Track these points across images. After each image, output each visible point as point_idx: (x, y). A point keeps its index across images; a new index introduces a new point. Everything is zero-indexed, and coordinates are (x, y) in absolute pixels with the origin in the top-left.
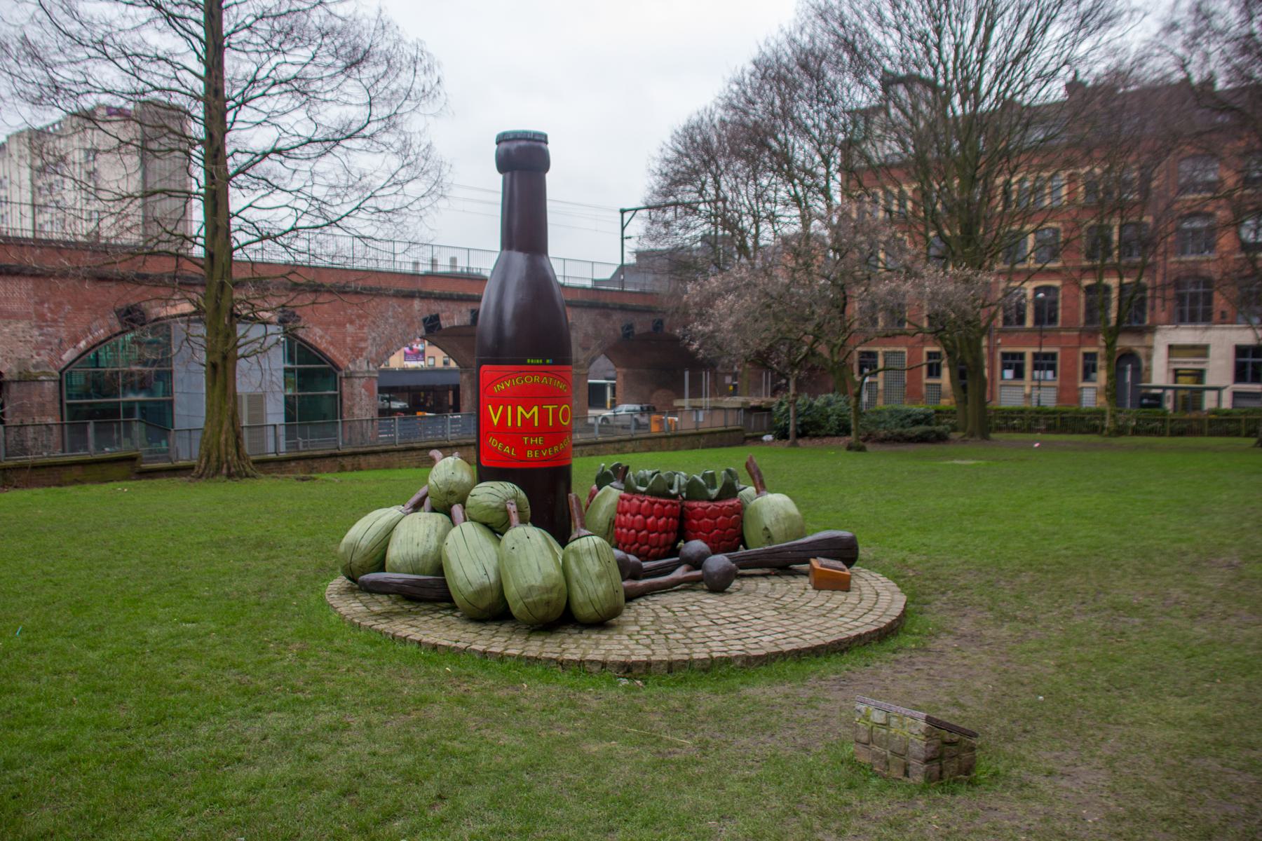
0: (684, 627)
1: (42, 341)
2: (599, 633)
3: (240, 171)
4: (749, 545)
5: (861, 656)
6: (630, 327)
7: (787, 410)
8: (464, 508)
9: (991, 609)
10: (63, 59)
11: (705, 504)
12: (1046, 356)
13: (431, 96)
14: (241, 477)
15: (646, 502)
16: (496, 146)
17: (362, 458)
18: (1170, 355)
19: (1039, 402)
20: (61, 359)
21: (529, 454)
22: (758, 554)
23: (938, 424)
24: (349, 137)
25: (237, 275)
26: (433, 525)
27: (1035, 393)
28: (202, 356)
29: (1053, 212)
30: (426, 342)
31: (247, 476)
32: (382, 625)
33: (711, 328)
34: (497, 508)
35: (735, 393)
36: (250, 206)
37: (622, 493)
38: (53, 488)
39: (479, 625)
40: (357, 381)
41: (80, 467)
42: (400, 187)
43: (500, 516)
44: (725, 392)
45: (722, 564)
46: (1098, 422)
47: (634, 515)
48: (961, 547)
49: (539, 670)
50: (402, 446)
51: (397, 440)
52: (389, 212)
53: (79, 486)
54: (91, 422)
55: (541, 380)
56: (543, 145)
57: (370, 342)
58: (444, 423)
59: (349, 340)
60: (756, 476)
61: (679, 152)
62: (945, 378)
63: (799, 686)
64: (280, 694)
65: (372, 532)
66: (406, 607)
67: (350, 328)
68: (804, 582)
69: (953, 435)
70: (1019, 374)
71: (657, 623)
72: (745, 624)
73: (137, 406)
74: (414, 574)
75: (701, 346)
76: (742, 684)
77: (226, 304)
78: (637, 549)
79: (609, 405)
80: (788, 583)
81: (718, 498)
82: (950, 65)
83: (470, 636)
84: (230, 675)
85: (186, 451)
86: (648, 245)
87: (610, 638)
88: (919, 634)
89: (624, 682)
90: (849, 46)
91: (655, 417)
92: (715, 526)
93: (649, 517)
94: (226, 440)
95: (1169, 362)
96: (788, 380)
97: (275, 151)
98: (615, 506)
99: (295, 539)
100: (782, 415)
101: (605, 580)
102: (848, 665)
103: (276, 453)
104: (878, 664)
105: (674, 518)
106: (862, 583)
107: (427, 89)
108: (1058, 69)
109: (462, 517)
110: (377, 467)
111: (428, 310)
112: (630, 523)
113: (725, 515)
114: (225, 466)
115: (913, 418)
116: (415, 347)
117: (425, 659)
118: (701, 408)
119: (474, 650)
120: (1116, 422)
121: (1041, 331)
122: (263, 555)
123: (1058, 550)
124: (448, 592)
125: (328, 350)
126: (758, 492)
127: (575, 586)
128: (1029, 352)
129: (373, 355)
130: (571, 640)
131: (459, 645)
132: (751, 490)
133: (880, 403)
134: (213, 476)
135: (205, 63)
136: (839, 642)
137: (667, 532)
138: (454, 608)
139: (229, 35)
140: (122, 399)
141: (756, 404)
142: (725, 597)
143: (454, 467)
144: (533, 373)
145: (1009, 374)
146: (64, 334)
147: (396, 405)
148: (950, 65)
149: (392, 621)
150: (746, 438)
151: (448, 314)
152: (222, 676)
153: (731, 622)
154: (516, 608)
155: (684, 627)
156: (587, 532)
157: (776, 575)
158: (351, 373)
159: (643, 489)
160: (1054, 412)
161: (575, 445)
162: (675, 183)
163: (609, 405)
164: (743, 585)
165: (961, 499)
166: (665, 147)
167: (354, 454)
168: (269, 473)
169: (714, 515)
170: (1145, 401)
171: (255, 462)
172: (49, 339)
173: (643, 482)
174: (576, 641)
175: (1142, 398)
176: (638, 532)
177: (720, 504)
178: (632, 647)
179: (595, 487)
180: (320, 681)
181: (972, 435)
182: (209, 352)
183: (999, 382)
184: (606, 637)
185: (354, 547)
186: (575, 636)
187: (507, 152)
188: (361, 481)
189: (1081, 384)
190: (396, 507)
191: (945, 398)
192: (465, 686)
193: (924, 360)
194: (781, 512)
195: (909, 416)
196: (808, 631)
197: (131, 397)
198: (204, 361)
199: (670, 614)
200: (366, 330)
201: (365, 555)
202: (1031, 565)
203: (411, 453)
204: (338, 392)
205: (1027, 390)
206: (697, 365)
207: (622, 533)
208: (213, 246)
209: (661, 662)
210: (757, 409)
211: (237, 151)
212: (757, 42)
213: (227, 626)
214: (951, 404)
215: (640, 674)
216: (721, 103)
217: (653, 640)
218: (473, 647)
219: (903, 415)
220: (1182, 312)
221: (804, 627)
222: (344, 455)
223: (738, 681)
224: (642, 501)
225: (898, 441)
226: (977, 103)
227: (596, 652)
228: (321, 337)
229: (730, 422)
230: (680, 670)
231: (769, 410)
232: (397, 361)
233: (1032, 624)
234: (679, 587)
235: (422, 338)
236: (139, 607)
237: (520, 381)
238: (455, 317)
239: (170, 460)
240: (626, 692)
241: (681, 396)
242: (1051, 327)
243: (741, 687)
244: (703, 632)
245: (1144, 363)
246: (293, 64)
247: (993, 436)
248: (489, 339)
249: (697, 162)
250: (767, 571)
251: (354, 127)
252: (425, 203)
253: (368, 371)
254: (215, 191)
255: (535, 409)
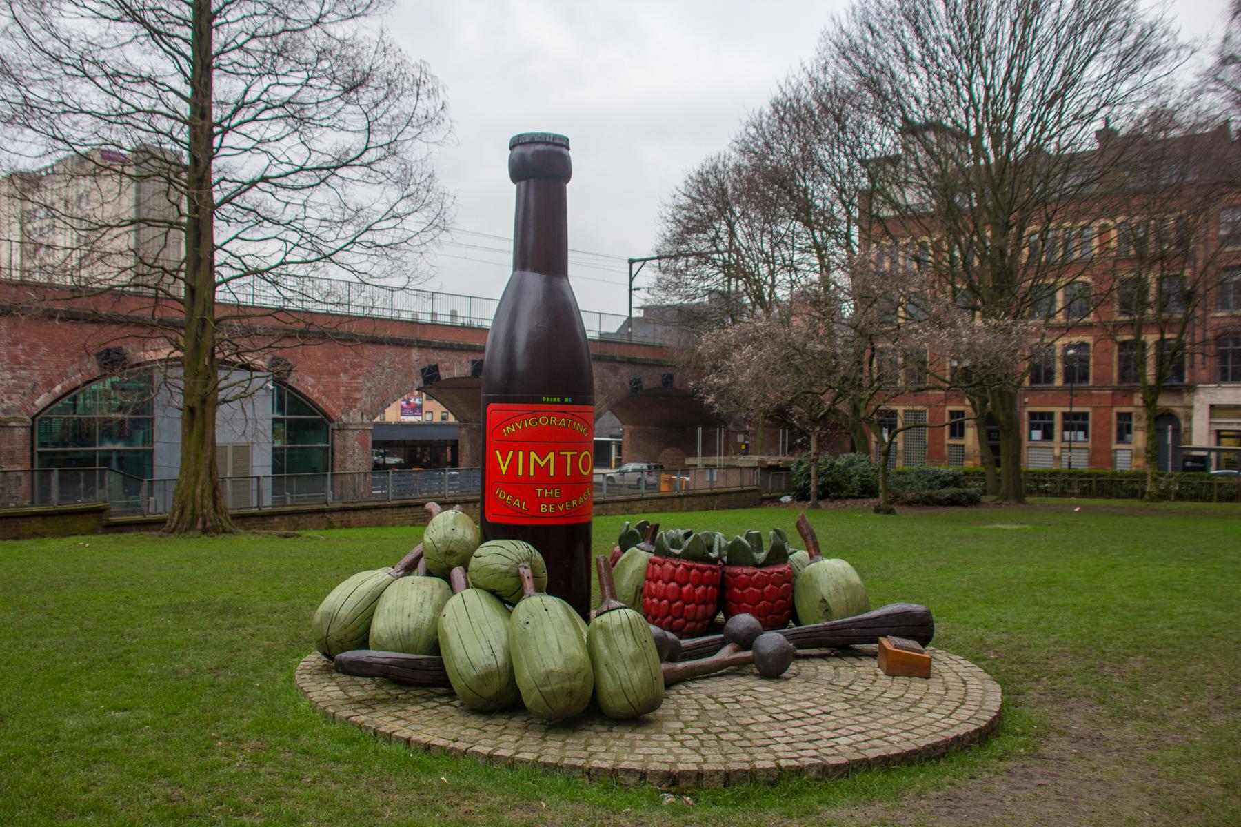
0: (738, 724)
1: (14, 385)
2: (633, 731)
3: (227, 200)
4: (802, 619)
5: (963, 765)
6: (638, 381)
7: (808, 469)
8: (466, 571)
9: (1102, 703)
10: (37, 76)
11: (750, 570)
12: (1077, 416)
13: (435, 122)
14: (218, 533)
15: (681, 567)
16: (510, 152)
17: (352, 515)
18: (1211, 416)
19: (1070, 464)
20: (34, 404)
21: (543, 508)
22: (816, 630)
23: (966, 486)
24: (346, 165)
25: (218, 314)
26: (429, 591)
27: (1066, 454)
28: (179, 399)
29: (1087, 265)
30: (424, 394)
31: (224, 532)
32: (363, 717)
33: (727, 380)
34: (507, 572)
35: (746, 453)
36: (236, 237)
37: (652, 556)
38: (8, 542)
39: (482, 718)
40: (350, 433)
41: (40, 519)
42: (399, 220)
43: (510, 582)
44: (738, 451)
45: (778, 643)
46: (1137, 487)
47: (667, 583)
48: (1043, 624)
49: (560, 781)
50: (395, 502)
51: (391, 497)
52: (386, 246)
53: (38, 539)
54: (56, 470)
55: (558, 421)
56: (564, 150)
57: (364, 392)
58: (441, 479)
59: (342, 389)
60: (809, 538)
61: (694, 199)
62: (971, 437)
63: (893, 808)
64: (220, 817)
65: (355, 599)
66: (393, 692)
67: (344, 378)
68: (870, 666)
69: (985, 499)
70: (1048, 435)
71: (704, 717)
72: (813, 720)
73: (114, 455)
74: (403, 652)
75: (716, 400)
76: (820, 802)
77: (206, 343)
78: (670, 623)
79: (613, 464)
80: (854, 667)
81: (766, 564)
82: (981, 106)
83: (471, 734)
84: (159, 789)
85: (159, 504)
86: (653, 300)
87: (648, 739)
88: (1023, 734)
89: (669, 799)
90: (872, 84)
91: (664, 476)
92: (762, 596)
93: (685, 585)
94: (203, 491)
95: (1210, 423)
96: (809, 437)
97: (264, 179)
98: (644, 571)
99: (267, 605)
100: (801, 475)
101: (641, 665)
102: (948, 778)
103: (258, 507)
104: (986, 776)
105: (713, 586)
106: (941, 667)
107: (431, 115)
108: (1097, 111)
109: (463, 582)
110: (367, 525)
111: (427, 360)
112: (662, 593)
113: (773, 584)
114: (200, 520)
115: (941, 479)
116: (412, 401)
117: (415, 763)
118: (715, 466)
119: (477, 753)
120: (1157, 486)
121: (1072, 389)
122: (228, 623)
123: (1162, 629)
124: (445, 675)
125: (320, 400)
126: (811, 556)
127: (603, 670)
128: (1058, 411)
129: (368, 407)
130: (598, 741)
131: (458, 745)
132: (801, 554)
133: (900, 464)
134: (186, 531)
135: (193, 86)
136: (934, 746)
137: (705, 603)
138: (452, 695)
139: (218, 55)
140: (98, 448)
141: (773, 463)
142: (781, 685)
143: (455, 522)
144: (549, 413)
145: (1037, 435)
146: (37, 378)
147: (391, 460)
148: (981, 106)
149: (375, 711)
150: (764, 499)
151: (447, 364)
152: (146, 790)
153: (795, 718)
154: (530, 698)
155: (738, 724)
156: (617, 604)
157: (836, 656)
158: (344, 425)
159: (678, 552)
160: (1089, 475)
161: (595, 503)
162: (689, 231)
163: (613, 464)
164: (800, 668)
165: (1022, 568)
166: (678, 193)
167: (344, 510)
168: (249, 529)
169: (760, 583)
170: (1188, 464)
171: (234, 517)
172: (22, 383)
173: (675, 543)
174: (605, 742)
175: (1185, 461)
176: (671, 602)
177: (768, 570)
178: (676, 751)
179: (618, 549)
180: (274, 797)
181: (1006, 498)
182: (186, 394)
183: (1026, 443)
184: (643, 737)
185: (332, 617)
186: (604, 735)
187: (522, 157)
188: (349, 539)
189: (1115, 446)
190: (385, 569)
191: (969, 459)
192: (466, 806)
193: (947, 420)
194: (841, 580)
195: (937, 477)
196: (893, 731)
197: (109, 446)
198: (181, 406)
199: (718, 706)
200: (361, 380)
201: (345, 627)
202: (1137, 647)
203: (405, 510)
204: (329, 445)
205: (1057, 452)
206: (712, 421)
207: (652, 603)
208: (194, 278)
209: (717, 772)
210: (775, 468)
211: (225, 179)
212: (777, 81)
213: (167, 716)
214: (975, 465)
215: (688, 788)
216: (738, 147)
217: (701, 741)
218: (475, 748)
219: (930, 477)
220: (1224, 371)
221: (886, 725)
222: (333, 511)
223: (814, 799)
224: (677, 566)
225: (927, 504)
226: (1012, 146)
227: (633, 758)
228: (313, 386)
229: (746, 482)
230: (740, 784)
231: (787, 469)
232: (392, 414)
233: (1160, 723)
234: (724, 671)
235: (419, 389)
236: (61, 689)
237: (533, 422)
238: (456, 368)
239: (142, 513)
240: (674, 814)
241: (693, 454)
242: (1082, 385)
243: (820, 808)
244: (763, 732)
245: (1183, 424)
246: (285, 85)
247: (1028, 499)
248: (498, 374)
249: (711, 208)
250: (825, 651)
251: (352, 155)
252: (425, 237)
253: (362, 424)
254: (198, 220)
255: (551, 455)
